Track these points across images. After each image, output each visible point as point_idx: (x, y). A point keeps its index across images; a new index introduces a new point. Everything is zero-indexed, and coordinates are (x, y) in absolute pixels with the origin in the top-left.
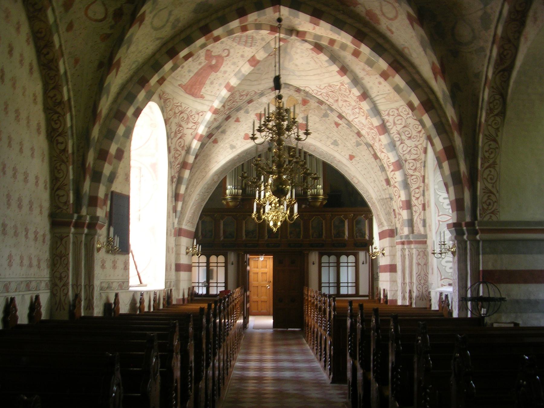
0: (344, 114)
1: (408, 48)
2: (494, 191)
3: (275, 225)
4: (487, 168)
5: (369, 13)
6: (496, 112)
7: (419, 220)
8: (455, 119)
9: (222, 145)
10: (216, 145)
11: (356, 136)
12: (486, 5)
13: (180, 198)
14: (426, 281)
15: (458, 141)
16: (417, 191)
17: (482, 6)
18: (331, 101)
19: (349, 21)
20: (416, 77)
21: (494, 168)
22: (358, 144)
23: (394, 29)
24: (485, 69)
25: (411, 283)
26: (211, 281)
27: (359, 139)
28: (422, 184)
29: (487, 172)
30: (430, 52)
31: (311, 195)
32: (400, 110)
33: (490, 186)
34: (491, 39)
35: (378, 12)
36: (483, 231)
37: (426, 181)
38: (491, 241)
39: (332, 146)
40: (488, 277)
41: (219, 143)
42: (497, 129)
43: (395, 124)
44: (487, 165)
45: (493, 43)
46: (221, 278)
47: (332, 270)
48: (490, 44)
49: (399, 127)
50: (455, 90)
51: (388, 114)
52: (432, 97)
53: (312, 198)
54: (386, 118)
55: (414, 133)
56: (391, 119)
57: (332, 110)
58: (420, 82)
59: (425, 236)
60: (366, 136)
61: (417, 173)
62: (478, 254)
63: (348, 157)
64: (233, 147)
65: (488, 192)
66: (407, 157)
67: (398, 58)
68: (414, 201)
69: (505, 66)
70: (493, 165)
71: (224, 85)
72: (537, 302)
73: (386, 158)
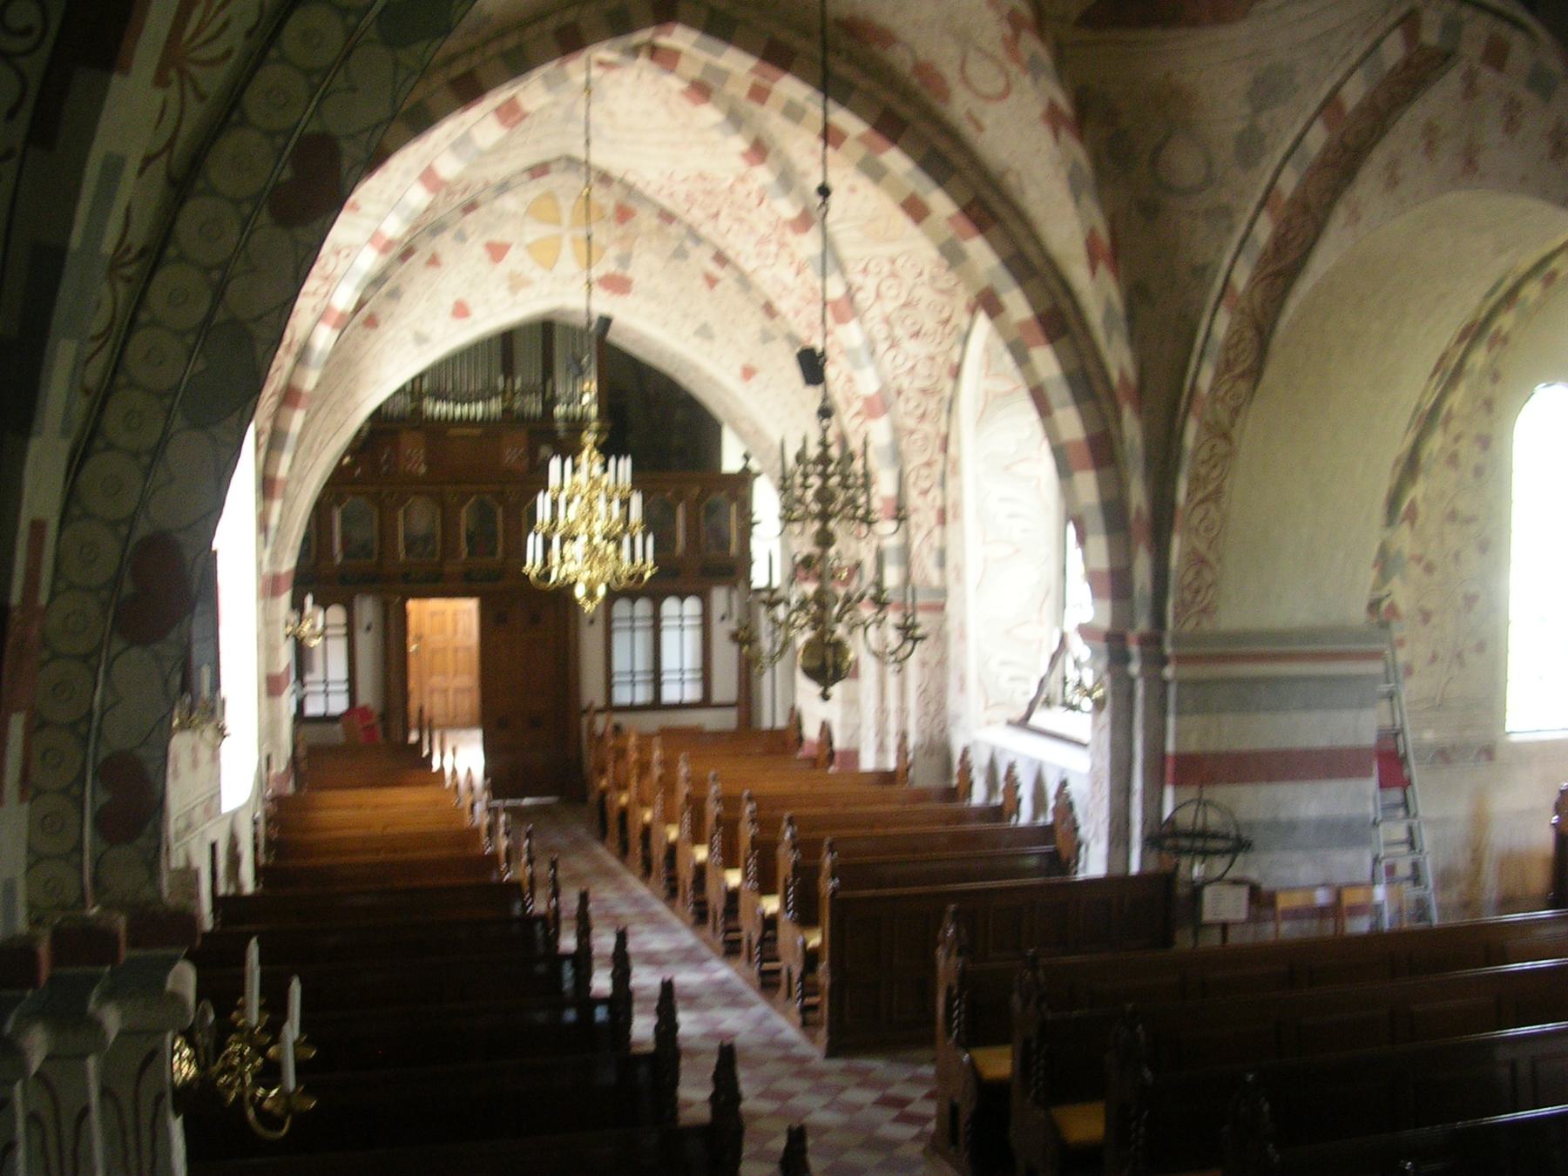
0: (730, 253)
1: (1019, 174)
2: (1211, 557)
3: (591, 594)
4: (1202, 501)
5: (925, 71)
6: (1238, 370)
7: (925, 550)
8: (1131, 375)
9: (390, 334)
10: (373, 334)
11: (760, 315)
12: (1257, 110)
13: (278, 490)
14: (941, 707)
15: (1132, 429)
16: (924, 472)
17: (1246, 110)
18: (696, 215)
19: (864, 83)
20: (1030, 249)
21: (1217, 501)
22: (766, 338)
23: (987, 121)
24: (1226, 261)
25: (903, 711)
26: (308, 678)
27: (768, 324)
28: (939, 457)
29: (1199, 513)
30: (1088, 202)
31: (566, 418)
32: (899, 262)
33: (1202, 547)
34: (1259, 195)
35: (950, 72)
36: (1181, 660)
37: (952, 449)
38: (1198, 683)
39: (696, 341)
40: (1192, 770)
41: (382, 328)
42: (1235, 412)
43: (878, 296)
44: (1200, 495)
45: (1262, 205)
46: (338, 669)
47: (642, 640)
48: (1252, 207)
49: (890, 306)
50: (1138, 297)
51: (865, 271)
52: (1065, 304)
53: (568, 430)
54: (857, 279)
55: (930, 324)
56: (870, 283)
57: (698, 240)
58: (1037, 261)
59: (943, 592)
60: (790, 316)
61: (927, 427)
62: (1163, 712)
63: (737, 371)
64: (421, 339)
65: (1198, 561)
66: (905, 382)
67: (986, 193)
68: (914, 499)
69: (1283, 267)
70: (1216, 495)
71: (417, 174)
72: (1292, 826)
73: (843, 378)
